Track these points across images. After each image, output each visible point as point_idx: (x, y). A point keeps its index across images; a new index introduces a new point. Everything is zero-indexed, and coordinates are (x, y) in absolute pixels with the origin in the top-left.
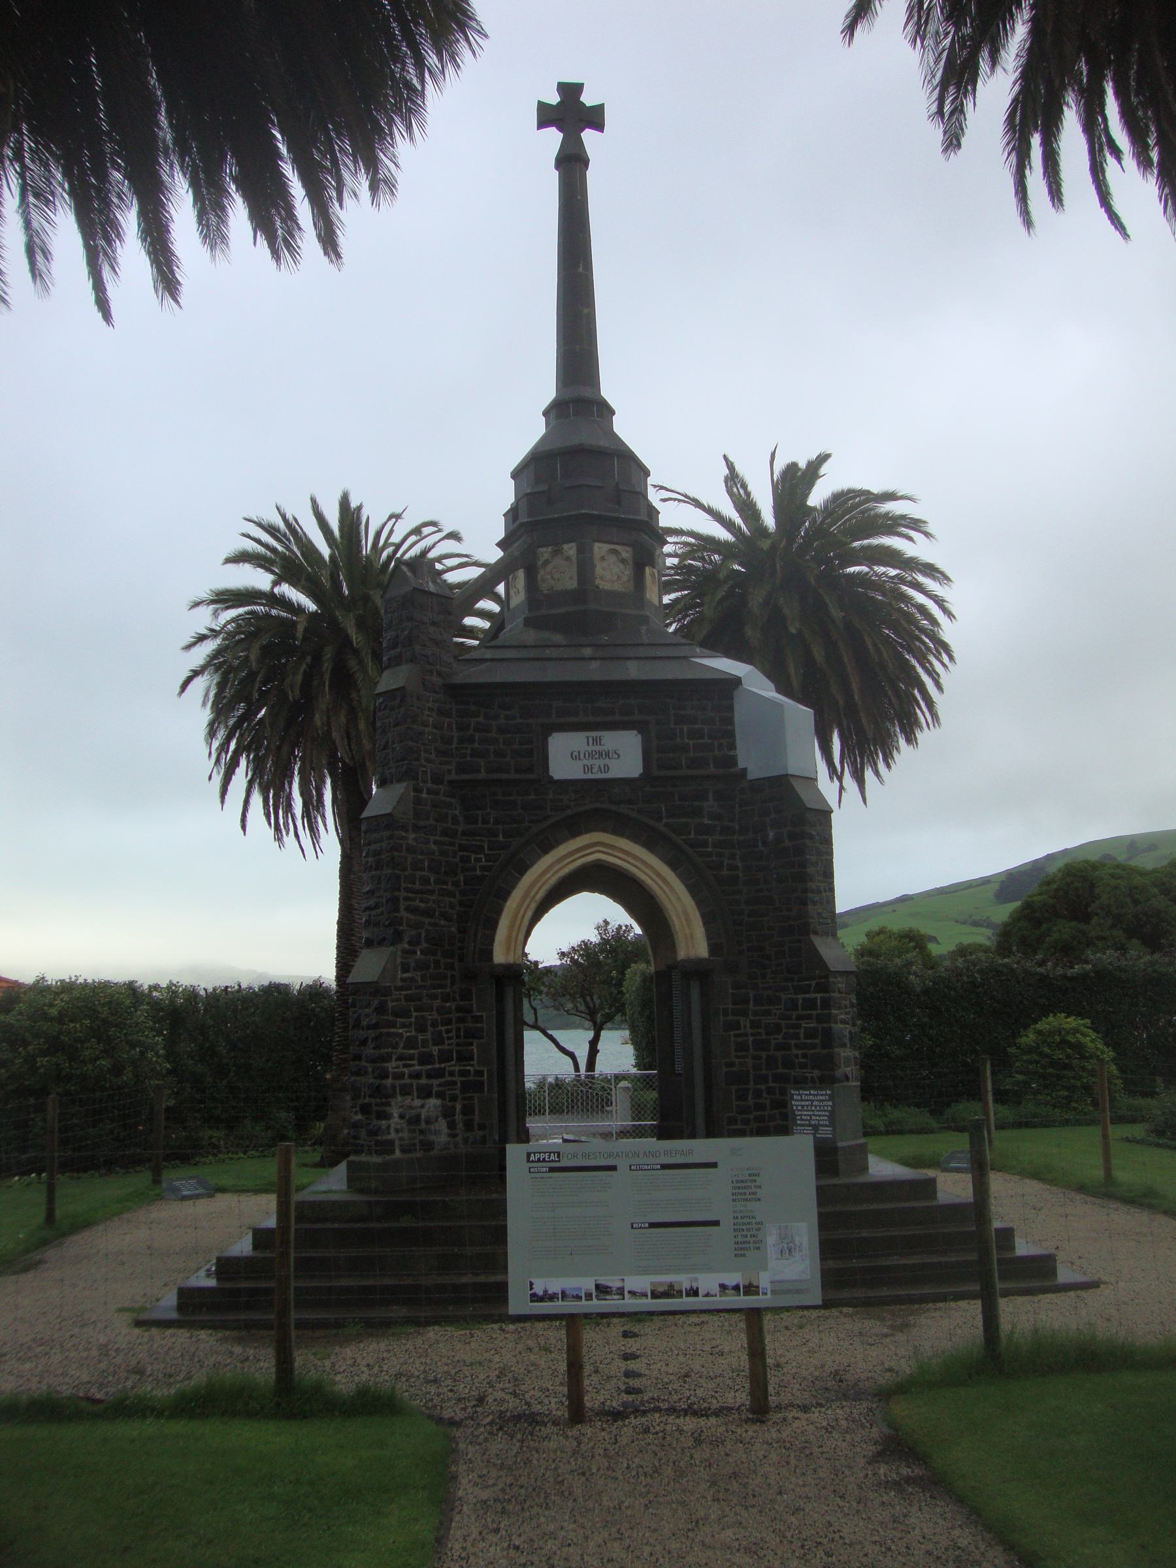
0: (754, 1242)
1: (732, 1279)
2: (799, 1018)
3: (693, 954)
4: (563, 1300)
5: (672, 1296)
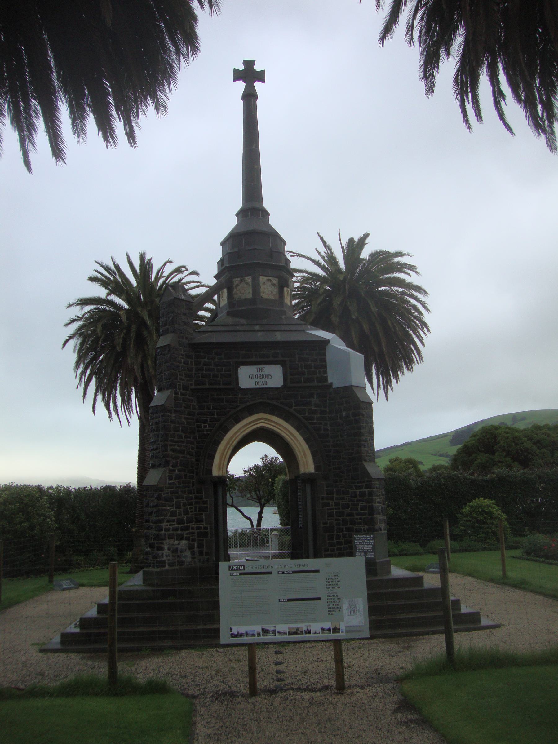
0: (337, 608)
1: (327, 625)
2: (358, 501)
3: (307, 471)
4: (246, 636)
5: (299, 634)
